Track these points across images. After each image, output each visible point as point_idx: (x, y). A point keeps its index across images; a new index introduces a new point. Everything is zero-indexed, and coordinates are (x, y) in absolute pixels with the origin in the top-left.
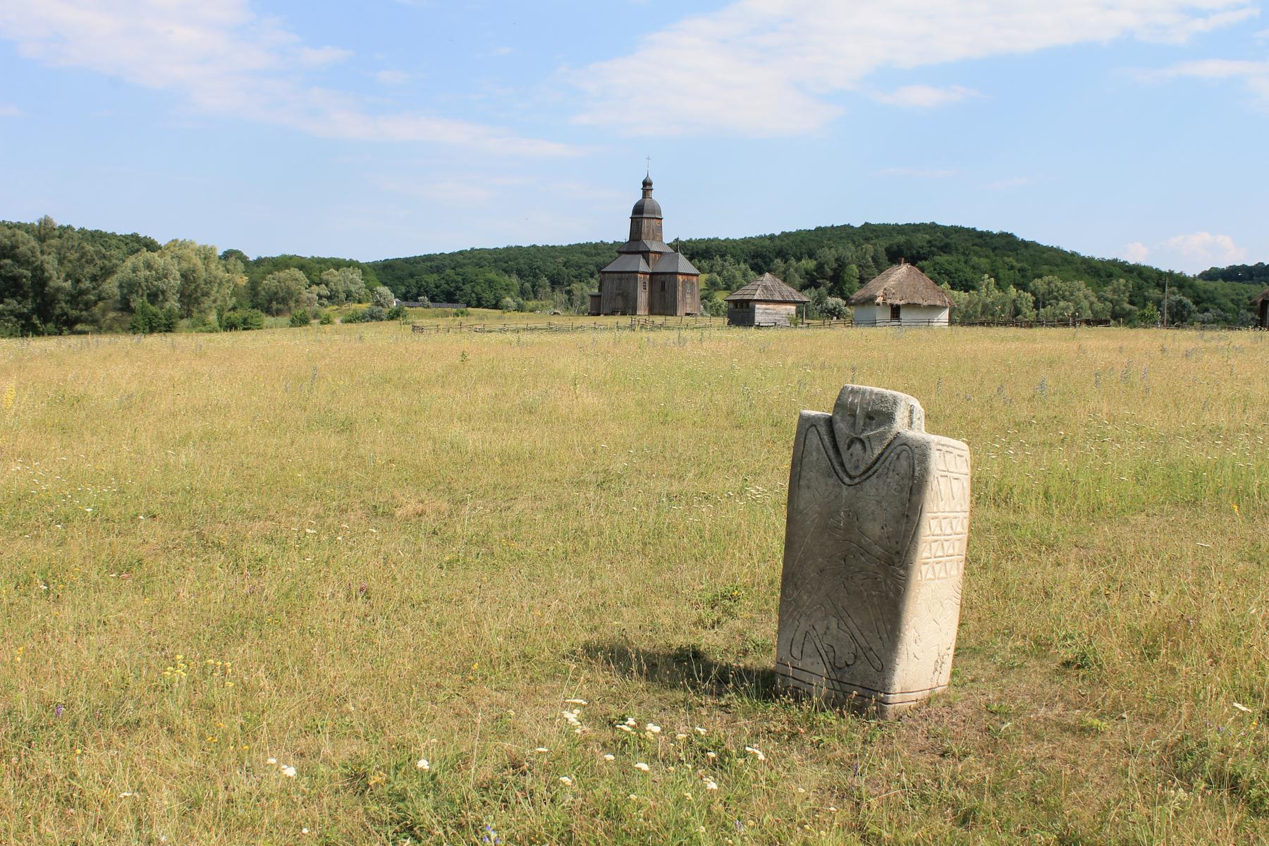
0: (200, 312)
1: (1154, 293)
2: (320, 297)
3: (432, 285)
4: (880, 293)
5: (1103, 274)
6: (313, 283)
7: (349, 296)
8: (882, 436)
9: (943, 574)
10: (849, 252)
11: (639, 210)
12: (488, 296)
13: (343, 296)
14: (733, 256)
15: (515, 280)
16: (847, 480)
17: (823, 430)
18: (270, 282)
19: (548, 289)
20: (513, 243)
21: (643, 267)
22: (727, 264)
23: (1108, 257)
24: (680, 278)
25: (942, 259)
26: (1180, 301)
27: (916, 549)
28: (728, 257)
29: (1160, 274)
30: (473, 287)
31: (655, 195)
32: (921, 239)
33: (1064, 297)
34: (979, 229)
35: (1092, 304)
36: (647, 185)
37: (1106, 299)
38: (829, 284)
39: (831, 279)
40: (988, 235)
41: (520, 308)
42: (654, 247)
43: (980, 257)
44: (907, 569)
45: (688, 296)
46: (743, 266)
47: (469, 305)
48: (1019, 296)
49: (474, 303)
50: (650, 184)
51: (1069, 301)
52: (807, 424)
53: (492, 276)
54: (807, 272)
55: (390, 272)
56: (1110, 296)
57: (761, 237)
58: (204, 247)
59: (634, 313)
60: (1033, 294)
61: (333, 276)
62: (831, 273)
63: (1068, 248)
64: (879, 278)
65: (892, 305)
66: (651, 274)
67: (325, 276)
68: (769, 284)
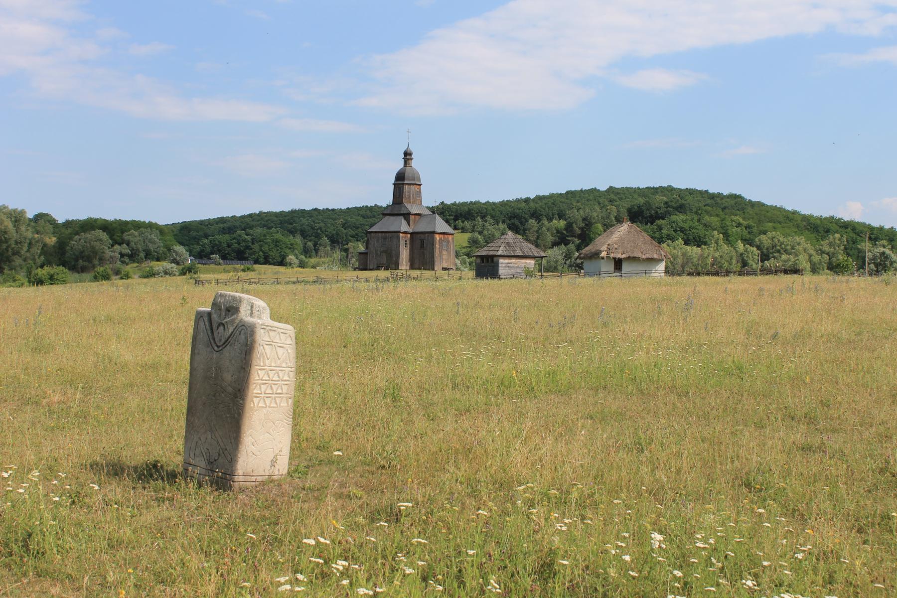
0: (11, 269)
1: (866, 245)
2: (122, 255)
3: (225, 245)
4: (604, 248)
5: (821, 230)
6: (115, 242)
7: (149, 255)
8: (233, 321)
9: (273, 405)
10: (596, 213)
11: (400, 177)
12: (274, 254)
13: (142, 255)
14: (492, 217)
15: (298, 240)
16: (216, 348)
17: (206, 319)
18: (77, 243)
19: (328, 248)
20: (297, 207)
21: (404, 227)
22: (487, 224)
23: (826, 214)
24: (437, 237)
25: (679, 218)
26: (883, 253)
27: (248, 388)
28: (488, 218)
29: (871, 229)
30: (261, 246)
31: (415, 164)
32: (658, 200)
33: (786, 251)
34: (711, 191)
35: (811, 256)
36: (407, 155)
37: (823, 252)
38: (577, 241)
39: (580, 237)
40: (720, 196)
41: (302, 265)
42: (414, 209)
43: (711, 215)
44: (243, 400)
45: (444, 253)
46: (501, 226)
47: (257, 262)
48: (746, 251)
49: (262, 260)
50: (411, 154)
51: (790, 254)
52: (200, 316)
53: (278, 236)
54: (558, 232)
55: (188, 233)
56: (827, 249)
57: (518, 201)
58: (15, 210)
59: (397, 268)
60: (758, 248)
61: (133, 236)
62: (579, 232)
63: (789, 207)
64: (605, 235)
65: (614, 258)
66: (412, 234)
67: (126, 237)
68: (511, 241)
